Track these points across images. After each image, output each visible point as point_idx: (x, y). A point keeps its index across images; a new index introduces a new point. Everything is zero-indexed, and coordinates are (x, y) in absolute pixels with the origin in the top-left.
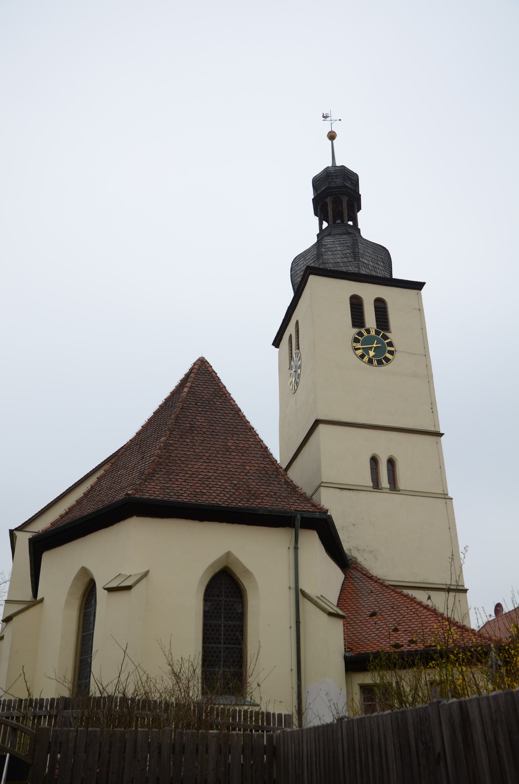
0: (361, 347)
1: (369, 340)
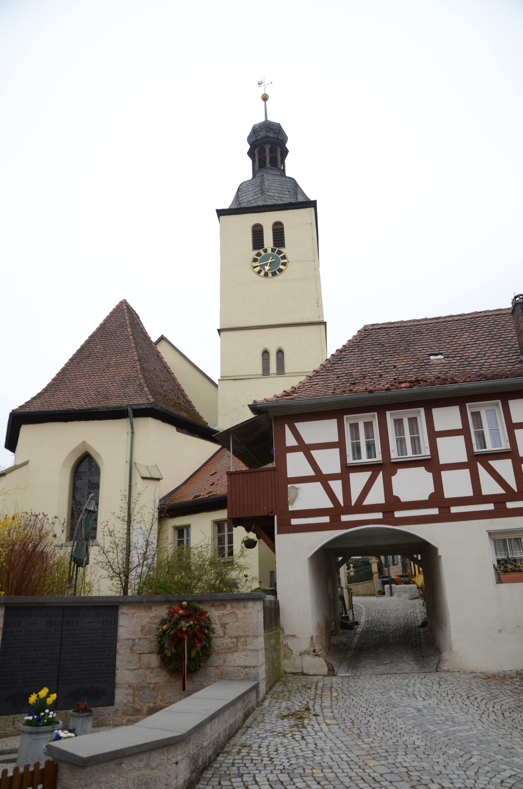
0: (258, 264)
1: (266, 258)
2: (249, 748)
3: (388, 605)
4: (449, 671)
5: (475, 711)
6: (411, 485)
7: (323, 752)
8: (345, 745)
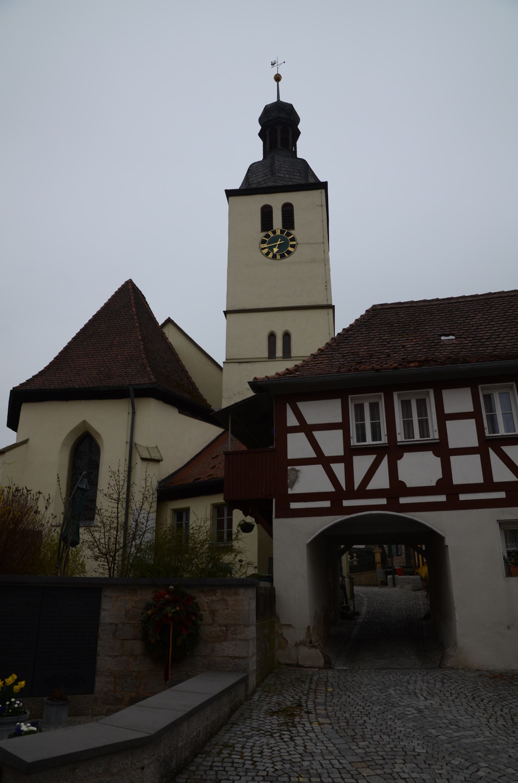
1: (275, 239)
2: (232, 749)
3: (398, 595)
4: (452, 668)
5: (481, 715)
6: (419, 469)
7: (313, 756)
8: (338, 749)
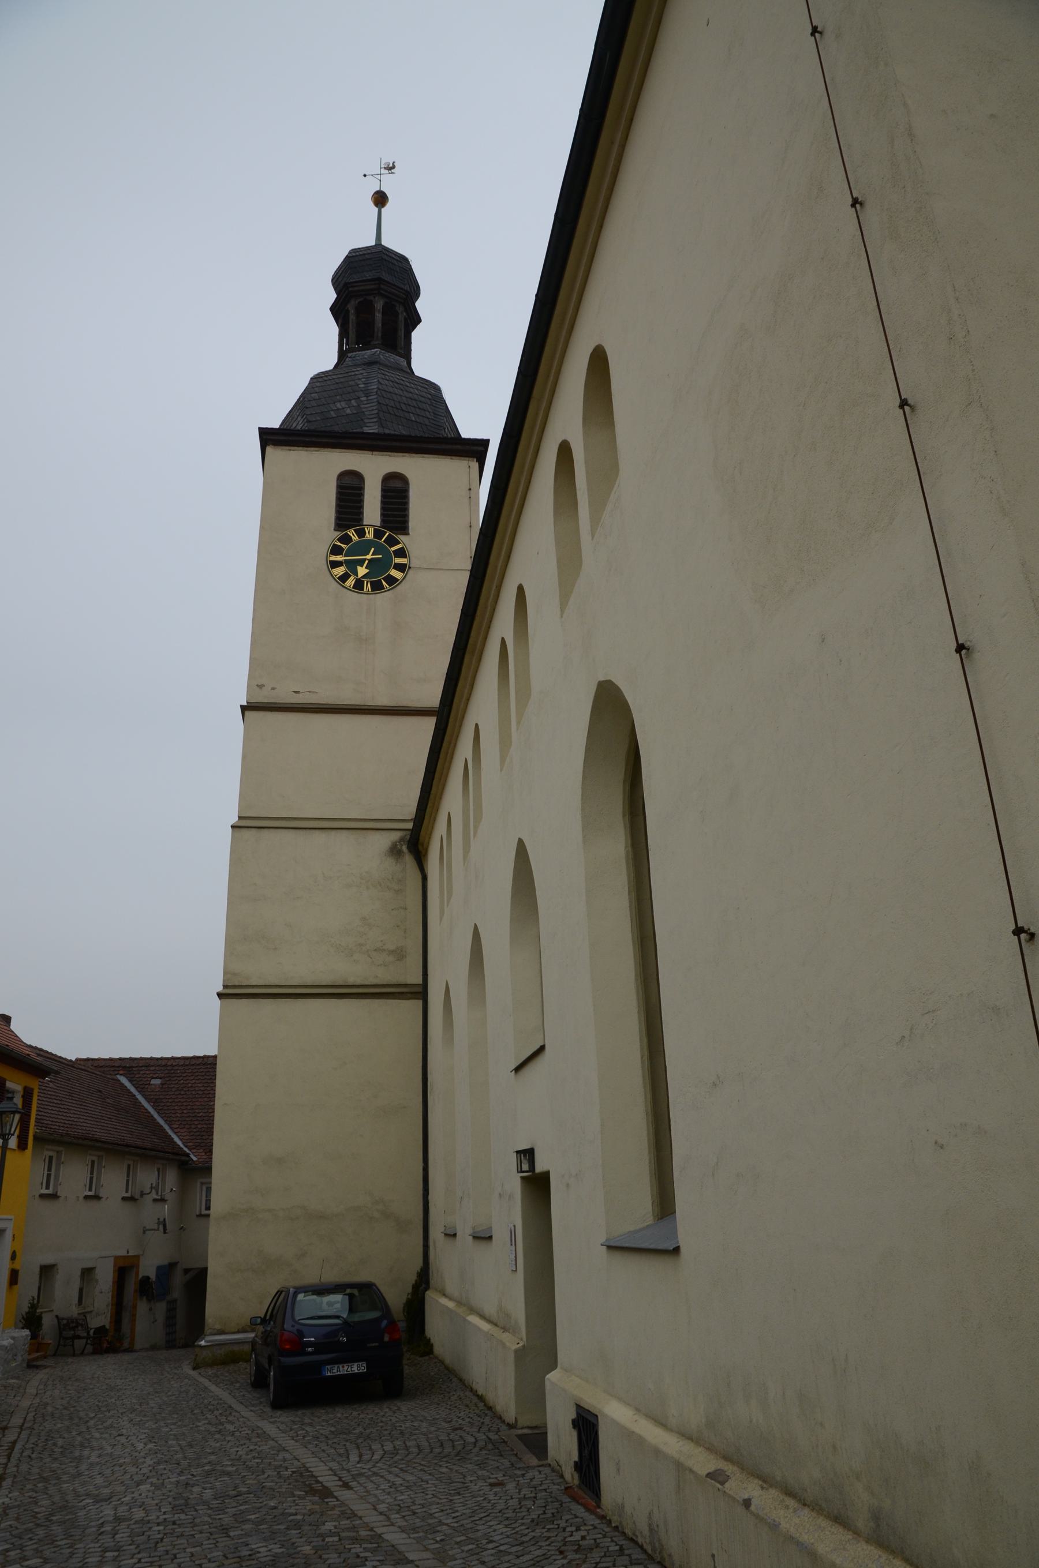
1: (363, 547)
